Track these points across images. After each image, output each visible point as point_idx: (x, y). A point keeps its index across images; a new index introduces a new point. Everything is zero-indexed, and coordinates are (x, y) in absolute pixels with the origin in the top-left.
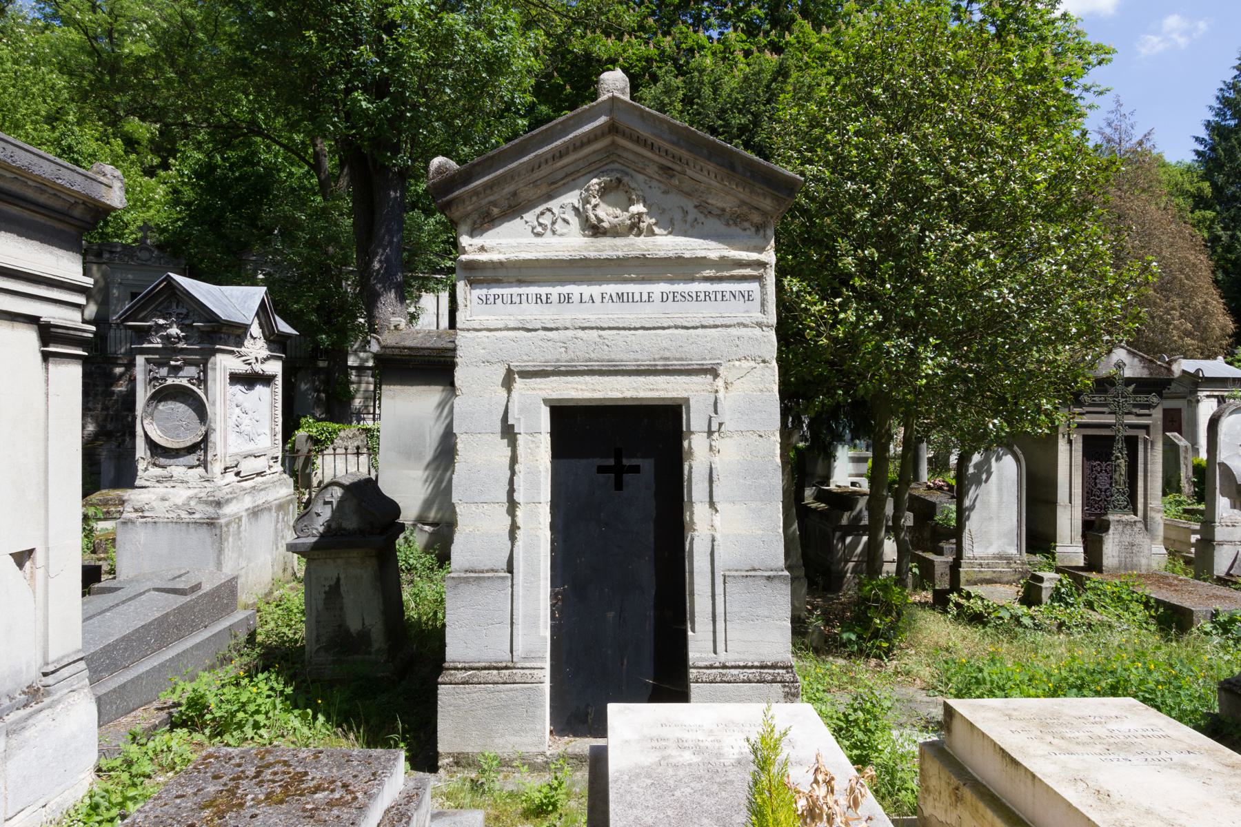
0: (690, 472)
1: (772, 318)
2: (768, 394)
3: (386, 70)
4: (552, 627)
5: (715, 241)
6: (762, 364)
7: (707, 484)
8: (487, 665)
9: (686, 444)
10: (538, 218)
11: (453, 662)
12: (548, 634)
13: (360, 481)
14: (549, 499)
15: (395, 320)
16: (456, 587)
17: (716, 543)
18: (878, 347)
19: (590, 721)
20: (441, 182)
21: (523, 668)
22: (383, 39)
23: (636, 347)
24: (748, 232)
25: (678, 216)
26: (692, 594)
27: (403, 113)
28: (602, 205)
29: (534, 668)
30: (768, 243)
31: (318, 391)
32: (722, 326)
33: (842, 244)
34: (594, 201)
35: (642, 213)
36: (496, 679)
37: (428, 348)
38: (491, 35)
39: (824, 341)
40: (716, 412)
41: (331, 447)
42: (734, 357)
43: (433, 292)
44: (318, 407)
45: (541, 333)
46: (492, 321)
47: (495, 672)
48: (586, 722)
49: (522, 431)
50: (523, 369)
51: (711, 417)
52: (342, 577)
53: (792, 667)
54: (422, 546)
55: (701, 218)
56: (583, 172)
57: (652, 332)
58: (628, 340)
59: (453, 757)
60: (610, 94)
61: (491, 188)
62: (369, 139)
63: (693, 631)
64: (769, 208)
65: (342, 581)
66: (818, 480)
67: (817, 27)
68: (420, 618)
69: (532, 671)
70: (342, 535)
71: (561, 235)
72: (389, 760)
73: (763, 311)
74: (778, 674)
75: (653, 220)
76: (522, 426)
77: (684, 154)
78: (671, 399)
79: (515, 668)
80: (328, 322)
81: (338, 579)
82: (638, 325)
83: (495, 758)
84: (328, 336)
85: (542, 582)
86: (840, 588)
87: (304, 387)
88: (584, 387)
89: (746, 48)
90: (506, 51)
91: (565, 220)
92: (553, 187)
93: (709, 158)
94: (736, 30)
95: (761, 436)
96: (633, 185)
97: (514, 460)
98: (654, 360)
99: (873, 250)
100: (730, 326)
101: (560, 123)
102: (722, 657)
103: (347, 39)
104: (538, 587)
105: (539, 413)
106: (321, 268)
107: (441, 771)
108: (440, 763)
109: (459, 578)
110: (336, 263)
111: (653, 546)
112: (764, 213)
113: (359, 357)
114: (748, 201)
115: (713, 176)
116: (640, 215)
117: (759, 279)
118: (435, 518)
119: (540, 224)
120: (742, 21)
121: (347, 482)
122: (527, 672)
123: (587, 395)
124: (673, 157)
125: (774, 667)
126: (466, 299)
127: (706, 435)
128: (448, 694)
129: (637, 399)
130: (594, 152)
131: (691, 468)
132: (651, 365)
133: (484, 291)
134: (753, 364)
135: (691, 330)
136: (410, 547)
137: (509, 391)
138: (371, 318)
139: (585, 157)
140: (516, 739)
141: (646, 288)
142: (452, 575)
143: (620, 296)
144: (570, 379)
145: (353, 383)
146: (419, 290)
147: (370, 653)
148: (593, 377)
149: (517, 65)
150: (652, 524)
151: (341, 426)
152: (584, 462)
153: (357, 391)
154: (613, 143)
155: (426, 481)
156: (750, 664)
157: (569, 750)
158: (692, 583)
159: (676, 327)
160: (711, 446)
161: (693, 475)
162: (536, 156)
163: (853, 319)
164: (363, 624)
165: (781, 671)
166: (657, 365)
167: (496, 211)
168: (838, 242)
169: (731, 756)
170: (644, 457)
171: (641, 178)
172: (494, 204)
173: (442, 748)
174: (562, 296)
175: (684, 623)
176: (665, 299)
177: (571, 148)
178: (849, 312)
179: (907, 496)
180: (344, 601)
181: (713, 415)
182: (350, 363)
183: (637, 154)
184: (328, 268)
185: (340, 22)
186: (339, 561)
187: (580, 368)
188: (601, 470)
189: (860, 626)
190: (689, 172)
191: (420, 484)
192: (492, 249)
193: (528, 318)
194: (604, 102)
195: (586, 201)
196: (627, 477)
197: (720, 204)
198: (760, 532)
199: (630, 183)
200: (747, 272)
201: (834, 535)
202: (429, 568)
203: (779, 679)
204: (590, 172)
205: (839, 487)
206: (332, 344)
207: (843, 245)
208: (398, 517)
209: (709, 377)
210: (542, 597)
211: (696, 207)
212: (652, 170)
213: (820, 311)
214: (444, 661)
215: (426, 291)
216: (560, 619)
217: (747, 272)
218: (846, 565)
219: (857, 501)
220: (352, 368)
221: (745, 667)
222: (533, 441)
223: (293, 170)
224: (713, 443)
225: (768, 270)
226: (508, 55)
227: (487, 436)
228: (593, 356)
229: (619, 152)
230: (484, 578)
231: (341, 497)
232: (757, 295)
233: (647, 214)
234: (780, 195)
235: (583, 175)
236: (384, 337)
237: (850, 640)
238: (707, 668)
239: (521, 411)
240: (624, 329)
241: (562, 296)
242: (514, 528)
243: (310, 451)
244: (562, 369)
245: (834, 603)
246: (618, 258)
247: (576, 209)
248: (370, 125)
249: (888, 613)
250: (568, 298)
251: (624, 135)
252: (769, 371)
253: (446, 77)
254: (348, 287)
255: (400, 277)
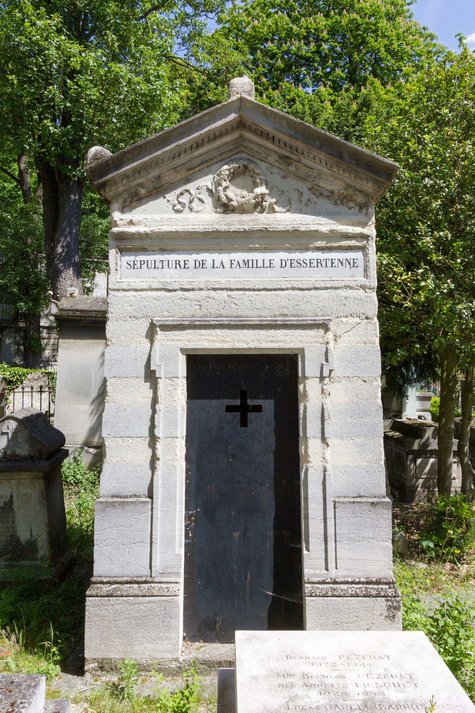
0: (305, 412)
1: (375, 283)
2: (370, 345)
3: (68, 105)
4: (186, 545)
5: (326, 217)
6: (365, 320)
7: (319, 422)
8: (129, 579)
9: (301, 387)
10: (178, 197)
11: (100, 577)
12: (182, 552)
13: (32, 416)
14: (185, 434)
15: (70, 290)
16: (103, 510)
17: (327, 473)
18: (451, 310)
19: (218, 628)
20: (97, 166)
21: (160, 583)
22: (67, 82)
23: (259, 305)
24: (353, 210)
25: (295, 196)
26: (307, 517)
27: (81, 137)
28: (232, 187)
29: (170, 583)
30: (370, 219)
31: (18, 344)
32: (332, 288)
33: (422, 227)
34: (224, 184)
35: (265, 194)
36: (137, 592)
37: (95, 311)
38: (148, 81)
39: (408, 304)
40: (327, 360)
41: (21, 386)
42: (342, 315)
43: (104, 272)
44: (18, 356)
45: (180, 293)
46: (139, 283)
47: (136, 586)
48: (213, 629)
49: (162, 376)
50: (164, 323)
51: (322, 365)
52: (15, 495)
53: (393, 583)
54: (87, 465)
55: (314, 198)
56: (215, 160)
57: (273, 292)
58: (253, 299)
59: (98, 662)
60: (239, 96)
61: (139, 172)
62: (56, 156)
63: (308, 550)
64: (370, 191)
65: (15, 499)
66: (393, 414)
67: (384, 84)
68: (82, 525)
69: (168, 585)
70: (16, 460)
71: (197, 212)
72: (29, 687)
73: (366, 275)
74: (382, 589)
75: (274, 200)
76: (163, 371)
77: (299, 144)
78: (289, 349)
79: (153, 582)
80: (26, 293)
81: (12, 497)
82: (261, 287)
83: (134, 666)
84: (26, 303)
85: (178, 507)
86: (412, 500)
87: (8, 341)
88: (215, 339)
89: (332, 99)
90: (158, 92)
91: (200, 200)
92: (191, 172)
93: (321, 148)
94: (325, 86)
95: (365, 381)
96: (257, 171)
97: (155, 401)
98: (275, 316)
99: (447, 231)
100: (338, 288)
101: (197, 118)
102: (333, 573)
103: (40, 83)
104: (175, 511)
105: (177, 360)
106: (22, 255)
107: (87, 675)
108: (86, 668)
109: (106, 502)
110: (33, 250)
111: (272, 475)
112: (366, 195)
113: (49, 319)
114: (353, 184)
115: (323, 163)
116: (263, 195)
117: (363, 249)
118: (98, 443)
119: (180, 203)
120: (329, 80)
121: (20, 416)
122: (164, 586)
123: (218, 345)
124: (291, 148)
125: (378, 582)
126: (116, 264)
127: (318, 380)
128: (94, 606)
129: (260, 349)
130: (226, 144)
131: (305, 408)
132: (272, 321)
133: (132, 258)
134: (358, 320)
135: (306, 292)
136: (78, 465)
137: (152, 342)
138: (54, 288)
139: (218, 148)
140: (151, 646)
141: (268, 256)
142: (100, 500)
143: (246, 263)
144: (203, 331)
145: (44, 338)
146: (94, 270)
147: (36, 559)
148: (223, 331)
149: (166, 103)
150: (272, 456)
151: (29, 370)
152: (214, 402)
153: (47, 344)
154: (241, 137)
155: (92, 413)
156: (357, 580)
157: (200, 656)
158: (307, 508)
159: (293, 289)
160: (323, 389)
161: (308, 414)
162: (176, 146)
163: (432, 286)
164: (31, 535)
165: (384, 587)
166: (277, 321)
167: (143, 191)
168: (419, 225)
169: (357, 697)
170: (265, 398)
171: (263, 165)
172: (141, 185)
173: (88, 654)
174: (197, 263)
175: (299, 541)
176: (284, 265)
177: (206, 140)
178: (429, 281)
179: (469, 428)
180: (16, 515)
181: (324, 363)
182: (42, 324)
183: (260, 145)
184: (27, 254)
185: (35, 69)
186: (13, 482)
187: (212, 323)
188: (229, 409)
189: (436, 535)
190: (303, 160)
191: (87, 416)
192: (139, 223)
193: (169, 280)
194: (233, 102)
195: (218, 184)
196: (251, 416)
197: (329, 187)
198: (365, 464)
199: (255, 169)
200: (353, 243)
201: (407, 458)
202: (92, 482)
203: (382, 594)
204: (221, 161)
205: (410, 419)
206: (29, 309)
207: (423, 228)
208: (63, 445)
209: (321, 331)
210: (177, 519)
211: (310, 189)
212: (272, 159)
213: (405, 279)
214: (92, 575)
215: (98, 272)
216: (193, 538)
217: (353, 243)
218: (417, 481)
219: (425, 431)
220: (44, 327)
221: (353, 583)
222: (171, 385)
223: (5, 185)
224: (325, 387)
225: (370, 242)
226: (160, 96)
227: (132, 379)
228: (223, 312)
229: (246, 144)
230: (127, 503)
231: (16, 429)
232: (361, 263)
233: (269, 195)
234: (379, 179)
235: (216, 163)
236: (62, 302)
237: (429, 547)
238: (319, 583)
239: (162, 358)
240: (249, 290)
241: (197, 263)
242: (154, 459)
243: (4, 389)
244: (197, 323)
245: (409, 513)
246: (245, 231)
247: (210, 191)
248: (57, 145)
249: (459, 525)
250: (202, 264)
251: (250, 130)
252: (371, 326)
253: (113, 111)
254: (42, 267)
255: (77, 259)
